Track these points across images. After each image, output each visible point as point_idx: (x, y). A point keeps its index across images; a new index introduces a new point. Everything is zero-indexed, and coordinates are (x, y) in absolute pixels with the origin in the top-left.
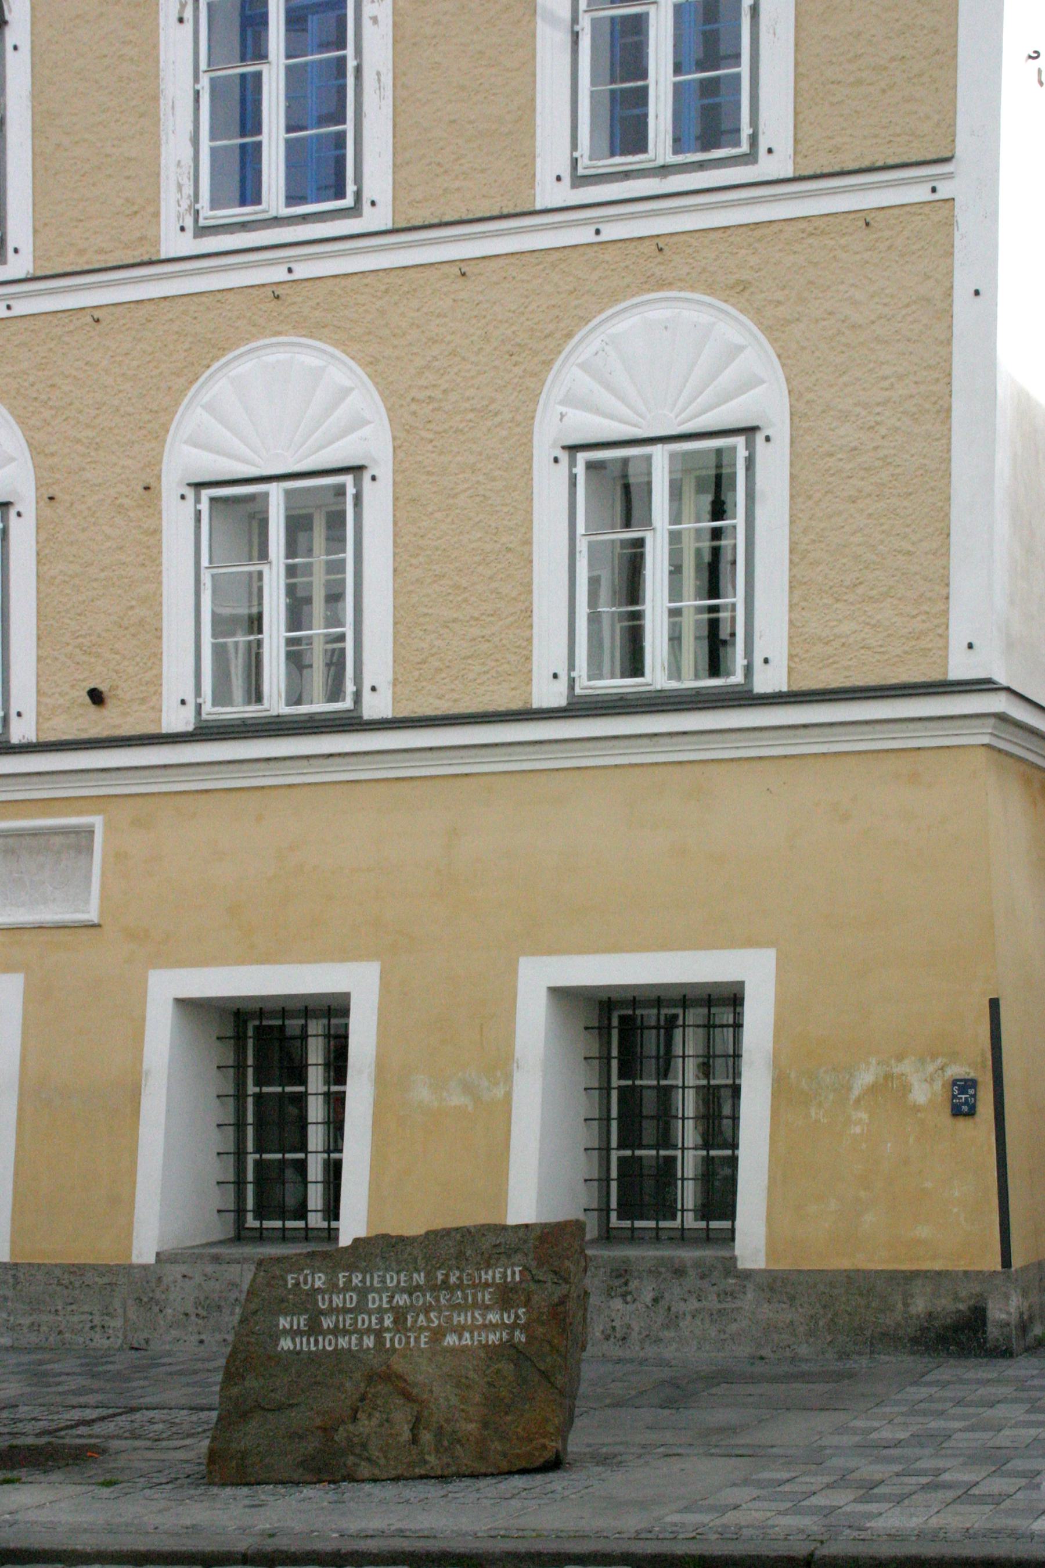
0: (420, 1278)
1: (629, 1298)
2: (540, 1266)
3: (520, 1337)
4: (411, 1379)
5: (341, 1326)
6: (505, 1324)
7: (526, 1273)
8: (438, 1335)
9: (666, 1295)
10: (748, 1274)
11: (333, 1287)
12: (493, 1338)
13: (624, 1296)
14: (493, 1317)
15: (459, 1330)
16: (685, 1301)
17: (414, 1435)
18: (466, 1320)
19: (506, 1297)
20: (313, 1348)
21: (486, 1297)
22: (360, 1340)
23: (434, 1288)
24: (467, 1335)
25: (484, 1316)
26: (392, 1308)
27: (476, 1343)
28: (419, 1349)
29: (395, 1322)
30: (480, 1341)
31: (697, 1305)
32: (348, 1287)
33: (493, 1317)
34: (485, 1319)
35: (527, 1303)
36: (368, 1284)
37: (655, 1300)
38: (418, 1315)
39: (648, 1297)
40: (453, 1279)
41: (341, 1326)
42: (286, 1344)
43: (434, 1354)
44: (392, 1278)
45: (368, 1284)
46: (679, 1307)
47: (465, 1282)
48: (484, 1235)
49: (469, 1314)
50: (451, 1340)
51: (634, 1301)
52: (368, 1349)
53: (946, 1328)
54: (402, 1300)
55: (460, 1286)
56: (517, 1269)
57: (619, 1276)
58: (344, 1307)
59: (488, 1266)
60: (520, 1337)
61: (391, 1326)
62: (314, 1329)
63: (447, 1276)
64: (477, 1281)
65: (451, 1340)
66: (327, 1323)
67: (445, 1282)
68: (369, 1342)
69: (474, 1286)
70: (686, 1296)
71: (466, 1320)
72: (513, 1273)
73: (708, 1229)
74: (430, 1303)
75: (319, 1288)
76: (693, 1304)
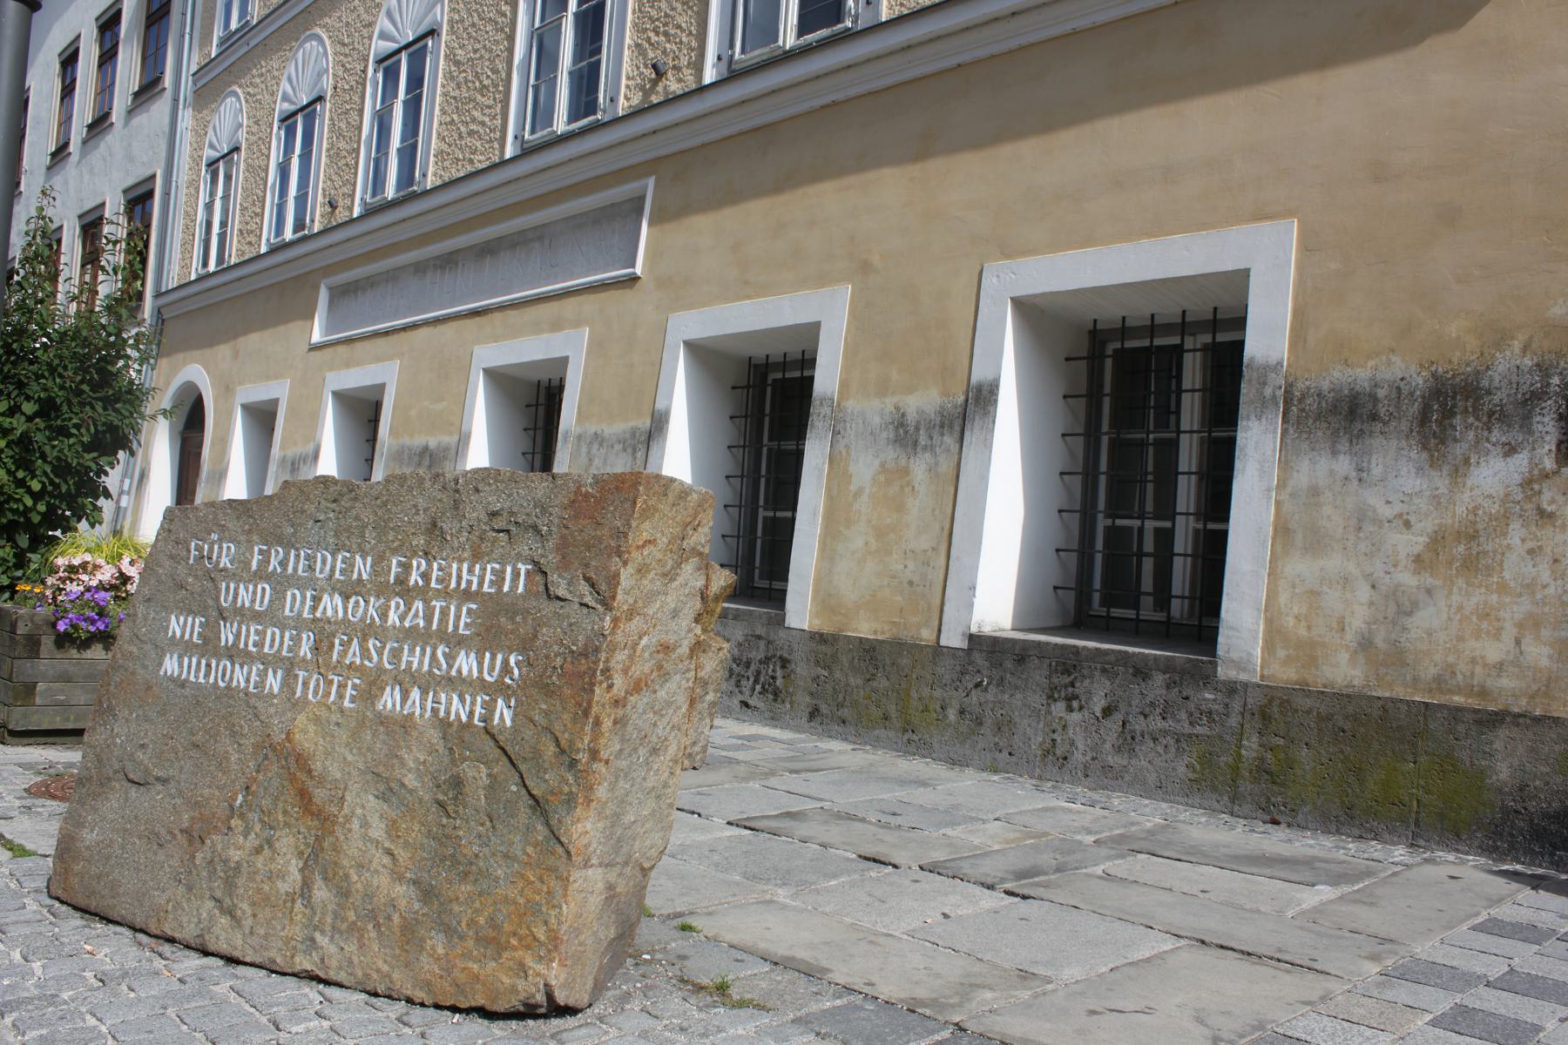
0: (363, 567)
1: (1075, 704)
2: (564, 564)
3: (504, 714)
4: (317, 766)
5: (242, 646)
6: (483, 680)
7: (539, 578)
8: (373, 685)
9: (1122, 706)
10: (1232, 688)
11: (244, 573)
12: (458, 709)
13: (1069, 699)
14: (466, 663)
15: (406, 680)
16: (1146, 716)
17: (304, 878)
18: (421, 663)
19: (496, 623)
20: (201, 680)
21: (462, 619)
22: (263, 675)
23: (383, 590)
24: (415, 694)
25: (450, 658)
26: (315, 620)
27: (428, 714)
28: (342, 711)
29: (316, 649)
30: (435, 711)
31: (1160, 724)
32: (261, 575)
33: (466, 663)
34: (450, 666)
35: (525, 646)
36: (290, 570)
37: (1108, 711)
38: (350, 641)
39: (1098, 704)
40: (414, 578)
41: (242, 646)
42: (170, 665)
43: (361, 724)
44: (324, 562)
45: (290, 570)
46: (1138, 724)
47: (433, 585)
48: (477, 490)
49: (499, 657)
50: (389, 700)
51: (1081, 708)
52: (272, 695)
53: (1545, 815)
54: (332, 605)
55: (423, 592)
56: (523, 568)
57: (1067, 672)
58: (251, 609)
59: (476, 556)
60: (504, 714)
61: (309, 656)
62: (208, 646)
63: (406, 567)
64: (453, 585)
65: (389, 700)
66: (227, 635)
67: (402, 581)
68: (274, 682)
69: (445, 594)
70: (1147, 710)
71: (421, 663)
72: (516, 574)
73: (1200, 626)
74: (372, 618)
75: (225, 569)
76: (1157, 723)
